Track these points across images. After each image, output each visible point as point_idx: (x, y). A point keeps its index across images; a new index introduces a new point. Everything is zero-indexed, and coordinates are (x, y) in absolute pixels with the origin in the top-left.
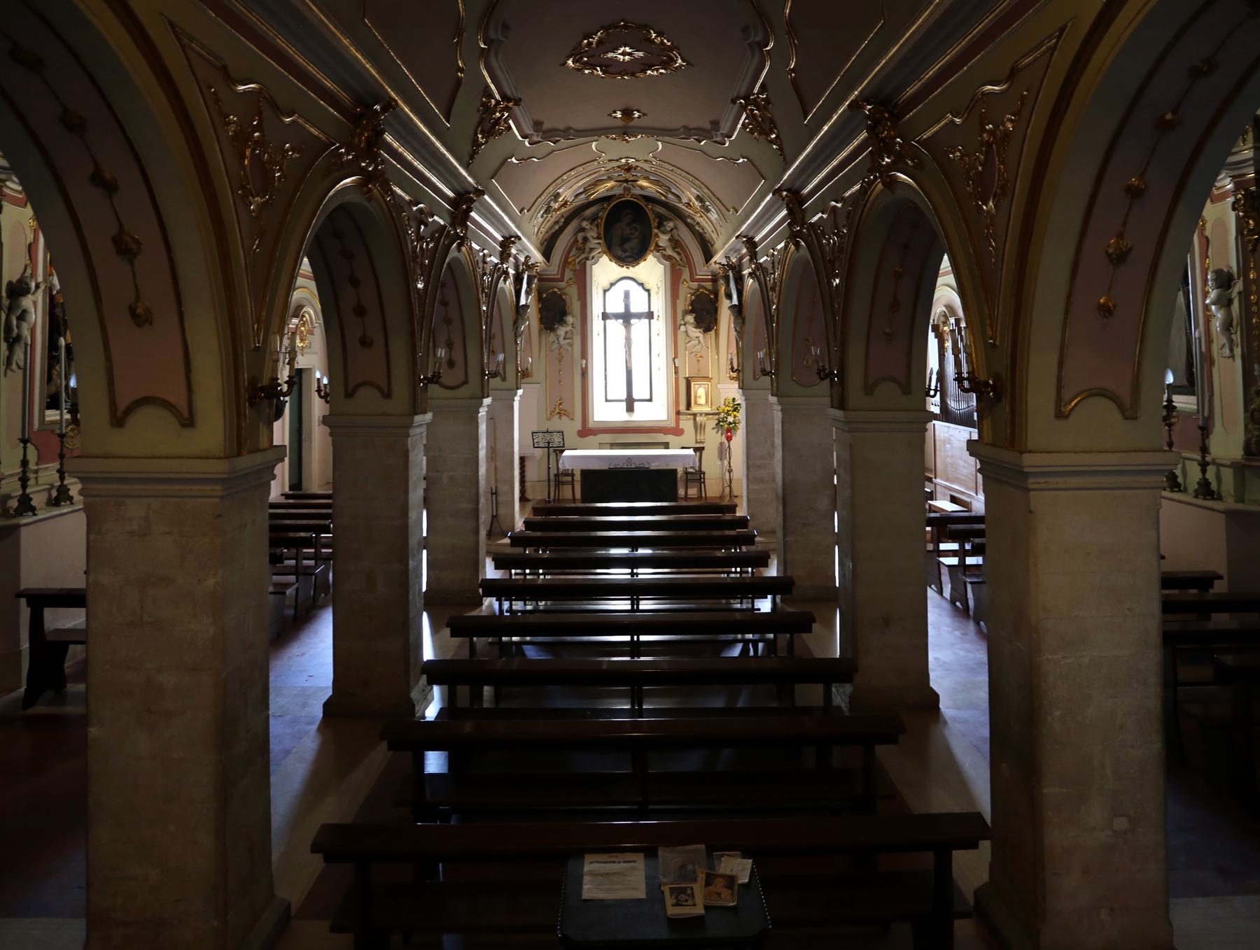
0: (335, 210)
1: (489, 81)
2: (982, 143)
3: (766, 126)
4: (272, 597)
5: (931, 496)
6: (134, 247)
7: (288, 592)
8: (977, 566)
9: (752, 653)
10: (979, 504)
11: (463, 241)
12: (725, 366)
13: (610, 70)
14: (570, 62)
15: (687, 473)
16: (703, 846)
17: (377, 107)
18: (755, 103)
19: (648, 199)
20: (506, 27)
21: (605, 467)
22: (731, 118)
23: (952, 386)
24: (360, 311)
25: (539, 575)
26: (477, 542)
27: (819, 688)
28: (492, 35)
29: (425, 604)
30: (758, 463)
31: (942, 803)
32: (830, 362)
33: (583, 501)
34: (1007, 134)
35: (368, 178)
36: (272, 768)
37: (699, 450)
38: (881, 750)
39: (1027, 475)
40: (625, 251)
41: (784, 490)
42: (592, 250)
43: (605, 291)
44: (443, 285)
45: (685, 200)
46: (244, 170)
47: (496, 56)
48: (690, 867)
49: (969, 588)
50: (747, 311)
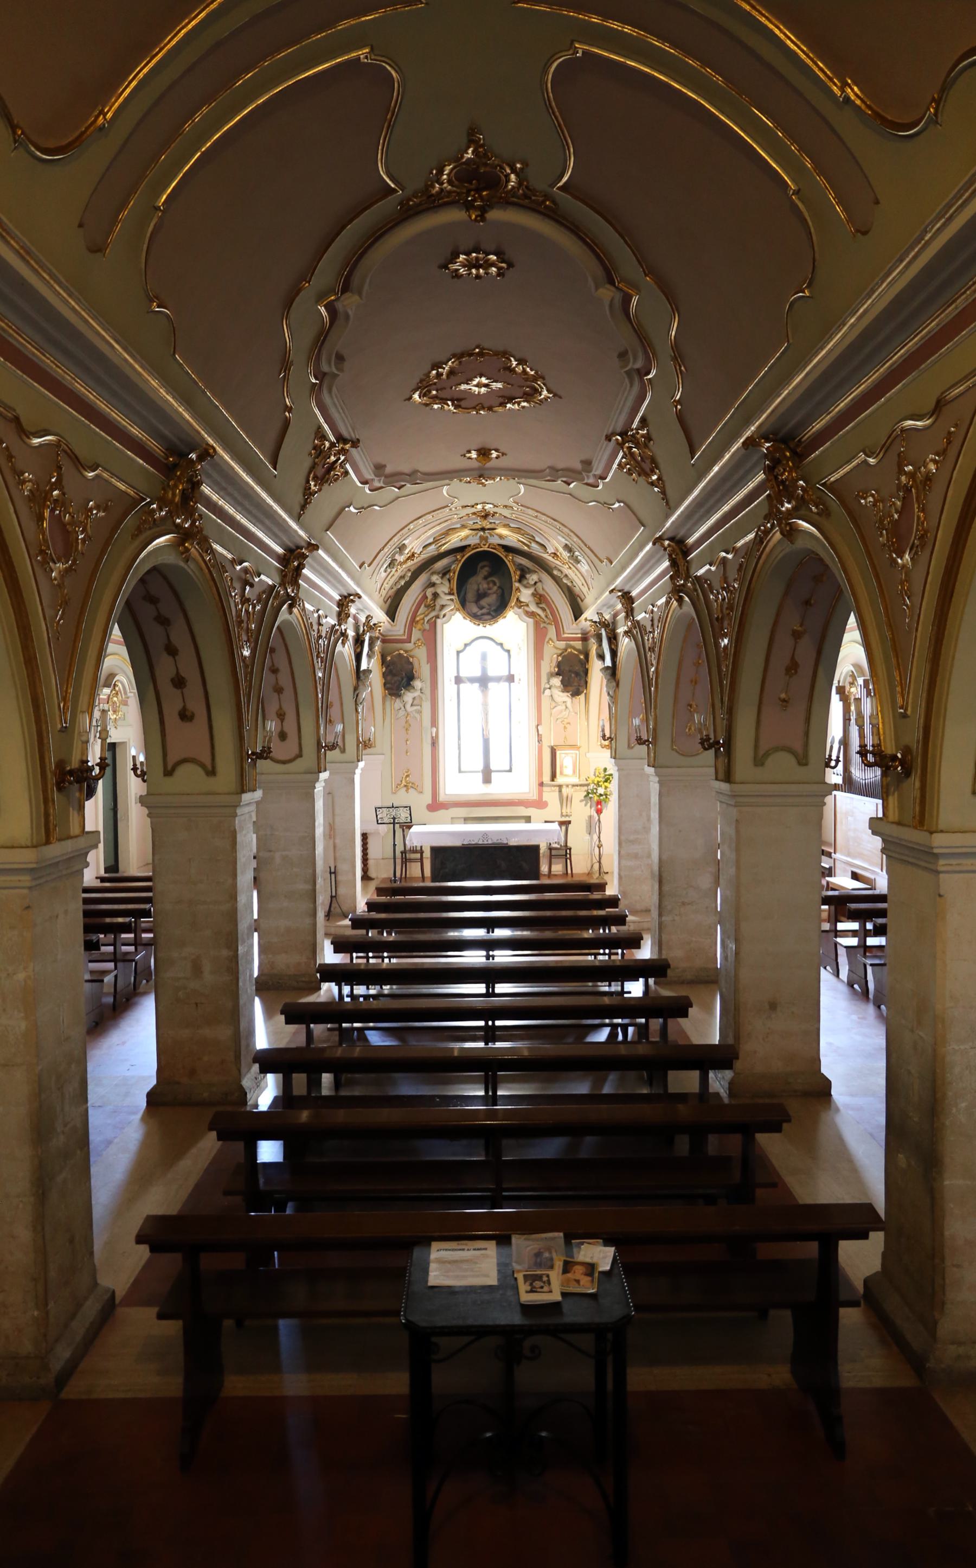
0: (149, 572)
1: (322, 420)
2: (899, 486)
3: (647, 466)
4: (88, 985)
5: (830, 872)
7: (106, 979)
8: (880, 947)
9: (620, 1038)
10: (882, 884)
11: (293, 602)
12: (595, 734)
13: (463, 403)
14: (416, 396)
15: (551, 849)
16: (561, 1234)
17: (193, 456)
18: (634, 439)
20: (340, 358)
21: (458, 843)
22: (606, 457)
23: (856, 759)
24: (179, 682)
25: (383, 958)
26: (315, 925)
27: (695, 1074)
28: (325, 368)
29: (257, 990)
30: (632, 837)
31: (828, 1191)
32: (715, 731)
33: (433, 880)
34: (929, 478)
35: (185, 536)
36: (92, 1159)
37: (565, 824)
38: (761, 1138)
39: (937, 856)
40: (481, 608)
41: (660, 868)
42: (443, 607)
43: (458, 653)
44: (273, 650)
45: (551, 550)
46: (44, 534)
47: (330, 391)
48: (547, 1255)
49: (869, 969)
50: (621, 673)
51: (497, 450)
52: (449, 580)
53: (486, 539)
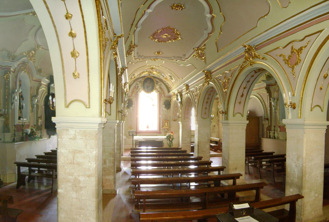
6: (77, 55)
19: (154, 77)
40: (148, 89)
41: (198, 143)
42: (139, 89)
45: (165, 77)
50: (183, 103)
51: (162, 52)
52: (141, 83)
53: (149, 74)
